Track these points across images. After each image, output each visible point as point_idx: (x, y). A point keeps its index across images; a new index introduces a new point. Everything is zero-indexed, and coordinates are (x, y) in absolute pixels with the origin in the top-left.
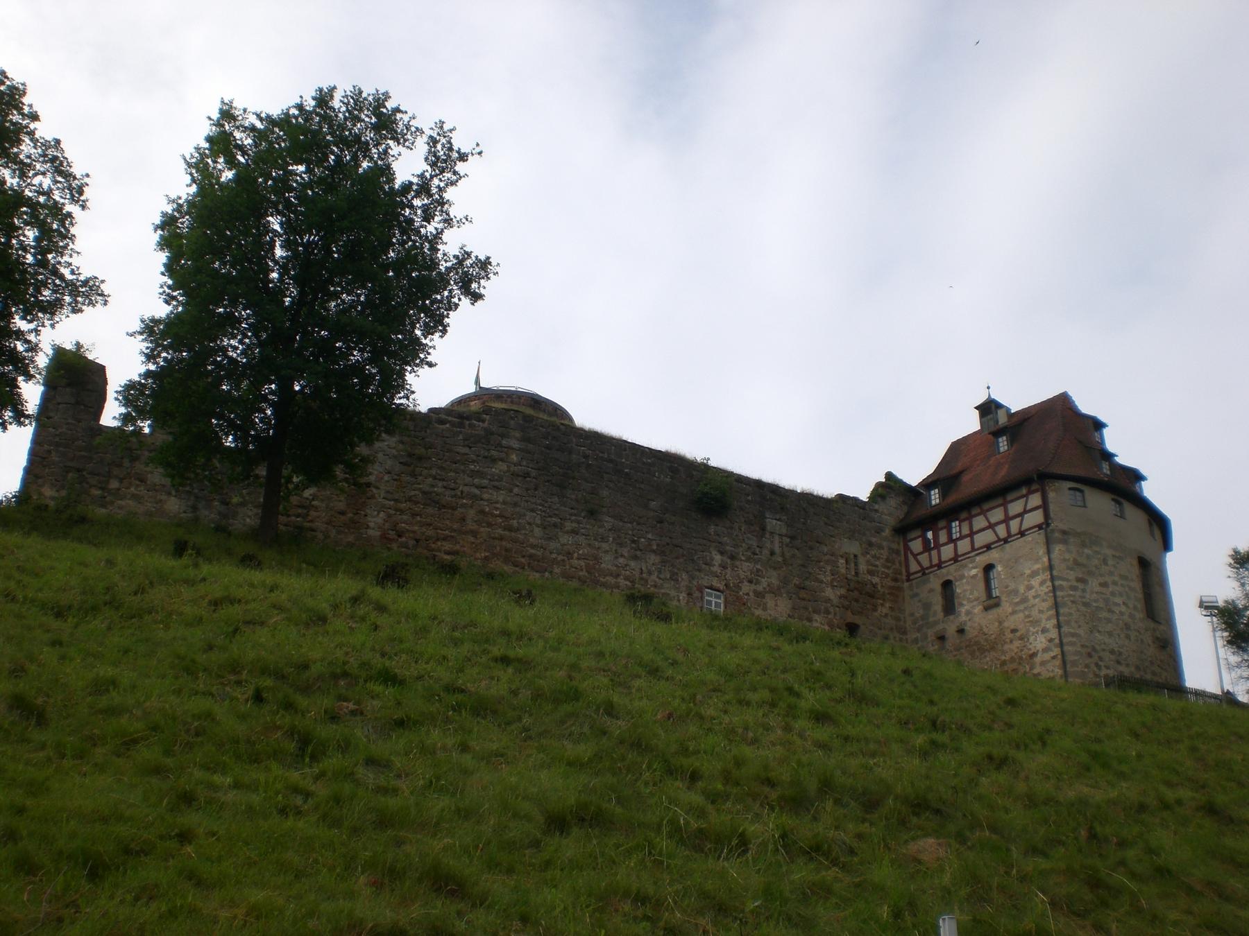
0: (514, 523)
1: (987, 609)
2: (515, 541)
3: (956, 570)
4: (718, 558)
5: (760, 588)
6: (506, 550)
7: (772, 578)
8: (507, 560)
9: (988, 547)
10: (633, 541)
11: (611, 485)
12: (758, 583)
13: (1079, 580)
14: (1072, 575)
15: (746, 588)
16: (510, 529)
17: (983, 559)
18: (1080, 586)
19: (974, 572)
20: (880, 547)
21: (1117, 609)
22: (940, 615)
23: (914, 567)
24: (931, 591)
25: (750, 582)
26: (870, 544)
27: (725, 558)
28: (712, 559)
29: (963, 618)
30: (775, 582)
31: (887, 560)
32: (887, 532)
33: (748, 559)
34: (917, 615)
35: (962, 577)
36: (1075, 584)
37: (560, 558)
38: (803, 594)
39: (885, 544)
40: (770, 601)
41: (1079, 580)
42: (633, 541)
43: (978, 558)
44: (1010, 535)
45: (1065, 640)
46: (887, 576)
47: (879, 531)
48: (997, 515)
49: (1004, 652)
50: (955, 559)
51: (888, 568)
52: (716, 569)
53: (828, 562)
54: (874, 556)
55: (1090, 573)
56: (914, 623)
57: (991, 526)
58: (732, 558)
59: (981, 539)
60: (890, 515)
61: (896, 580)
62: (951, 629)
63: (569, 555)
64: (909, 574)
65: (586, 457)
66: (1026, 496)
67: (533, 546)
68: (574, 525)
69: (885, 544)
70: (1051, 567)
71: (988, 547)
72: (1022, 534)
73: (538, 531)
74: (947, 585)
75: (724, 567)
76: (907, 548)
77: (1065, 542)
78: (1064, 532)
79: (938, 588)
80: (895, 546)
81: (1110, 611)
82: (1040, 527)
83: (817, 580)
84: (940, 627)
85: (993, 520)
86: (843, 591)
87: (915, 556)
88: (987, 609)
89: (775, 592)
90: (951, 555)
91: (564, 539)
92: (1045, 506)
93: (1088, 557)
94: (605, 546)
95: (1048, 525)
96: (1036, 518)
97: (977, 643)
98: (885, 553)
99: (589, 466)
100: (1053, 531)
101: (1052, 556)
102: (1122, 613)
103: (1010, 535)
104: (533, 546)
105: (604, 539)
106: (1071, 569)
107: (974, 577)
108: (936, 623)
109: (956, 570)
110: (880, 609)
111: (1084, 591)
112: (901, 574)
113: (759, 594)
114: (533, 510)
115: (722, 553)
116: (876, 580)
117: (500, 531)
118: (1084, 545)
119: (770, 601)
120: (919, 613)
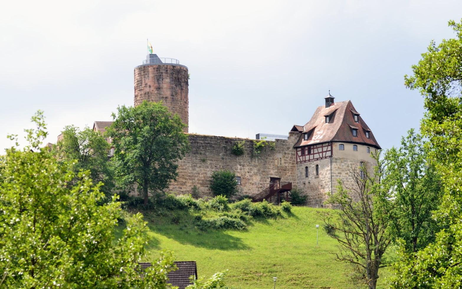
0: (184, 167)
1: (315, 178)
2: (185, 172)
3: (309, 164)
4: (239, 167)
5: (251, 174)
6: (183, 175)
7: (255, 170)
8: (183, 178)
9: (317, 159)
10: (216, 167)
11: (209, 151)
12: (251, 172)
13: (339, 173)
14: (337, 172)
15: (247, 174)
16: (183, 169)
17: (316, 162)
18: (339, 175)
19: (313, 166)
20: (289, 154)
21: (350, 181)
22: (304, 177)
23: (299, 160)
24: (302, 169)
25: (248, 173)
26: (285, 153)
27: (241, 167)
28: (238, 168)
29: (310, 179)
30: (256, 171)
31: (291, 158)
32: (291, 149)
33: (248, 166)
34: (299, 175)
35: (310, 167)
36: (337, 174)
37: (197, 175)
38: (264, 173)
39: (290, 153)
40: (254, 178)
41: (339, 173)
42: (216, 167)
43: (315, 162)
44: (323, 157)
45: (333, 191)
46: (290, 163)
47: (288, 148)
48: (320, 150)
49: (319, 191)
50: (309, 160)
51: (291, 160)
52: (239, 170)
53: (271, 162)
54: (287, 158)
55: (343, 171)
56: (298, 177)
57: (319, 153)
58: (243, 166)
59: (317, 156)
60: (292, 142)
61: (293, 164)
62: (307, 182)
63: (199, 174)
64: (297, 162)
65: (202, 144)
66: (327, 146)
67: (189, 173)
68: (200, 165)
69: (290, 153)
70: (331, 170)
71: (317, 159)
72: (326, 158)
73: (191, 169)
74: (307, 168)
75: (241, 169)
76: (297, 153)
77: (336, 162)
78: (336, 159)
79: (304, 169)
80: (293, 153)
81: (348, 181)
82: (330, 157)
83: (269, 168)
84: (304, 180)
85: (319, 151)
86: (276, 171)
87: (299, 156)
88: (315, 178)
89: (256, 174)
90: (308, 159)
91: (197, 169)
92: (332, 151)
93: (343, 166)
94: (208, 169)
95: (332, 157)
96: (329, 154)
97: (313, 187)
98: (290, 156)
99: (203, 146)
100: (333, 159)
101: (332, 166)
102: (351, 181)
103: (323, 157)
104: (189, 173)
105: (208, 167)
106: (337, 170)
107: (313, 167)
108: (303, 179)
109: (309, 164)
110: (287, 174)
111: (340, 176)
112: (295, 161)
113: (251, 176)
114: (189, 163)
115: (240, 165)
116: (287, 165)
117: (181, 170)
118: (342, 162)
119: (254, 178)
120: (299, 175)
